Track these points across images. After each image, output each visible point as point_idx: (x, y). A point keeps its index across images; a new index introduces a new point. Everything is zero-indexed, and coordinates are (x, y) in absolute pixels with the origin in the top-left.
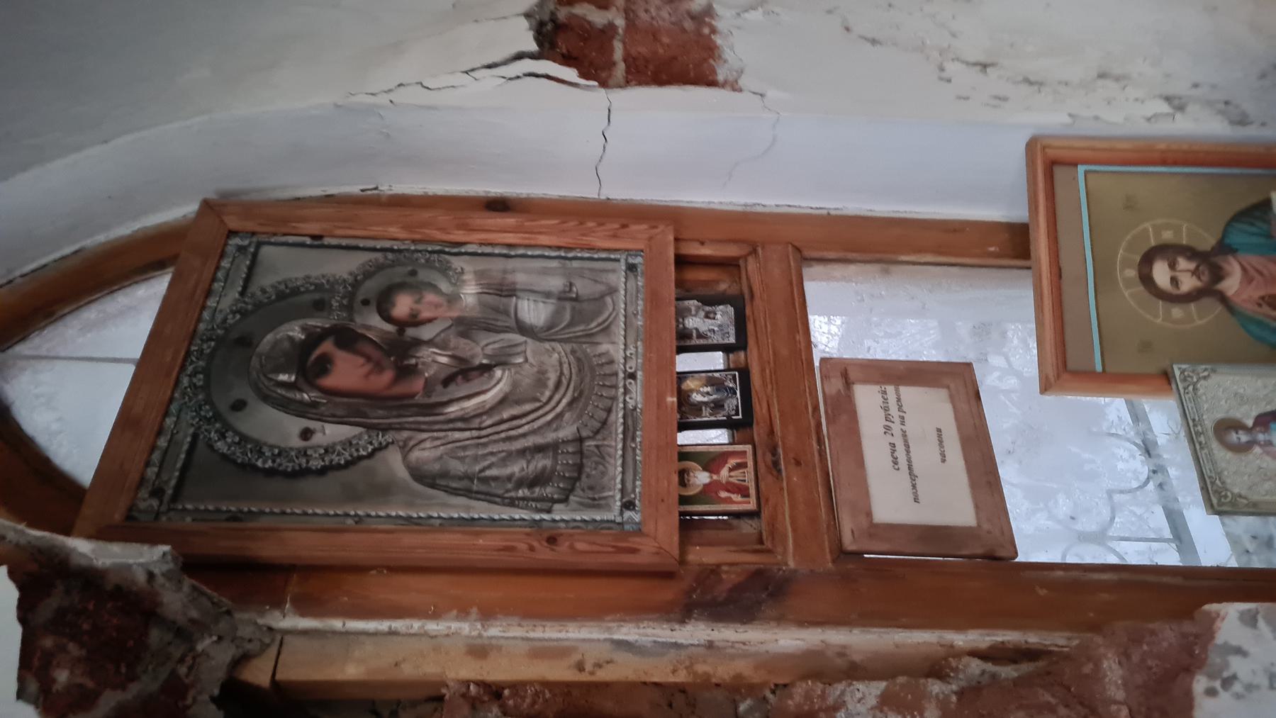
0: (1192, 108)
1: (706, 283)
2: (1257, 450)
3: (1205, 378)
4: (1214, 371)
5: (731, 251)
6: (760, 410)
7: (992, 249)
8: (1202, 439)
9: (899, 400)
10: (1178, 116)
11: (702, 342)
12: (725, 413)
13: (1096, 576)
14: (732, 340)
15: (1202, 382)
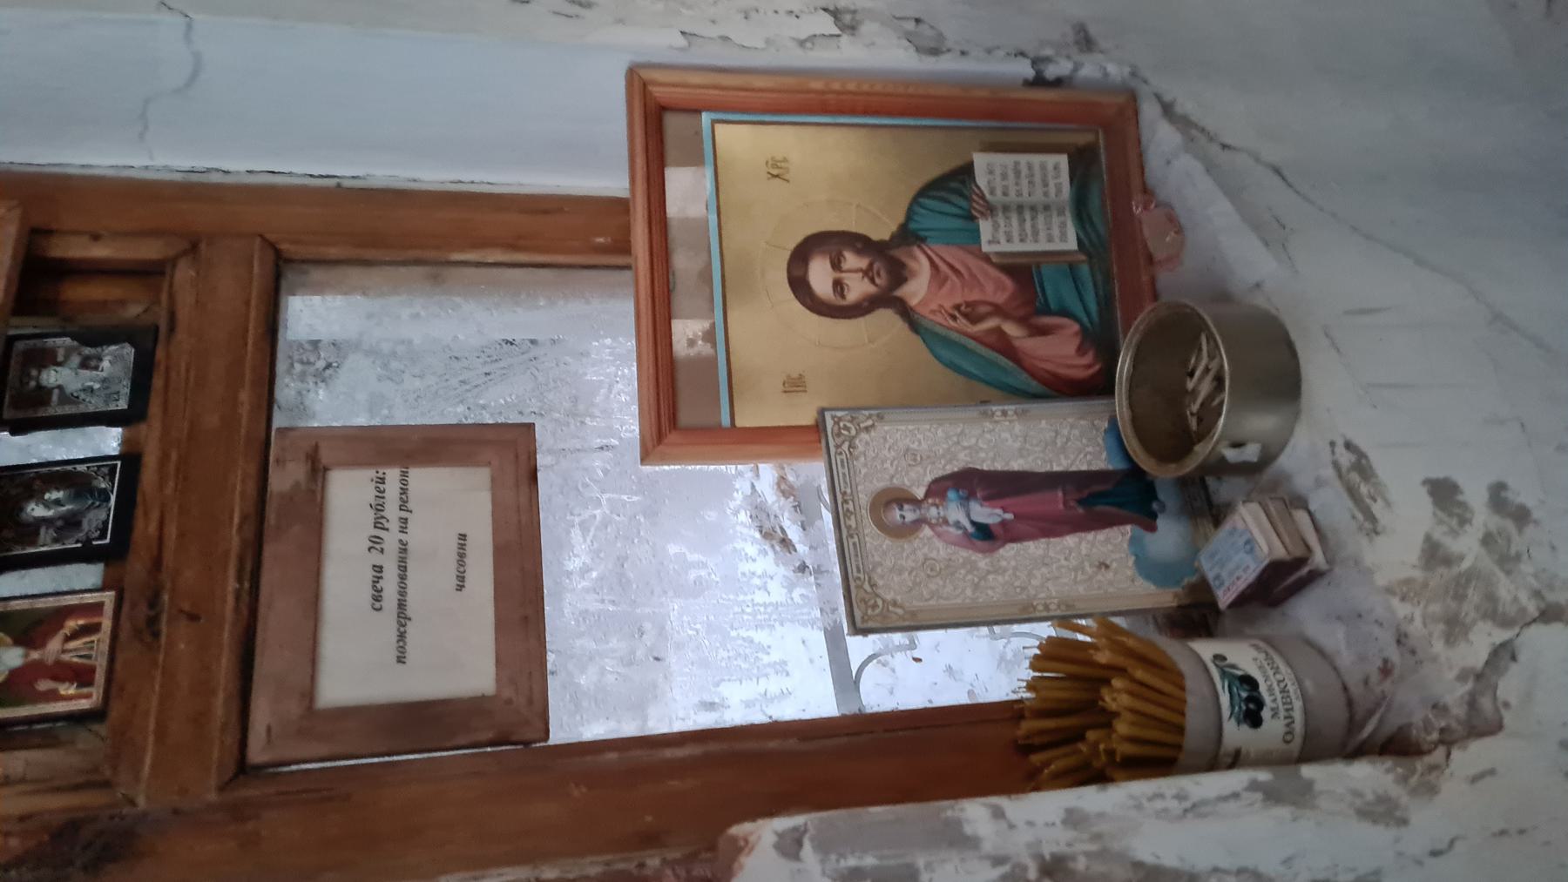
0: (868, 28)
1: (103, 305)
2: (927, 531)
3: (867, 429)
4: (880, 418)
5: (149, 251)
6: (144, 528)
7: (601, 240)
8: (852, 523)
9: (404, 491)
10: (845, 39)
11: (68, 410)
12: (81, 535)
13: (669, 753)
14: (123, 404)
15: (864, 436)
